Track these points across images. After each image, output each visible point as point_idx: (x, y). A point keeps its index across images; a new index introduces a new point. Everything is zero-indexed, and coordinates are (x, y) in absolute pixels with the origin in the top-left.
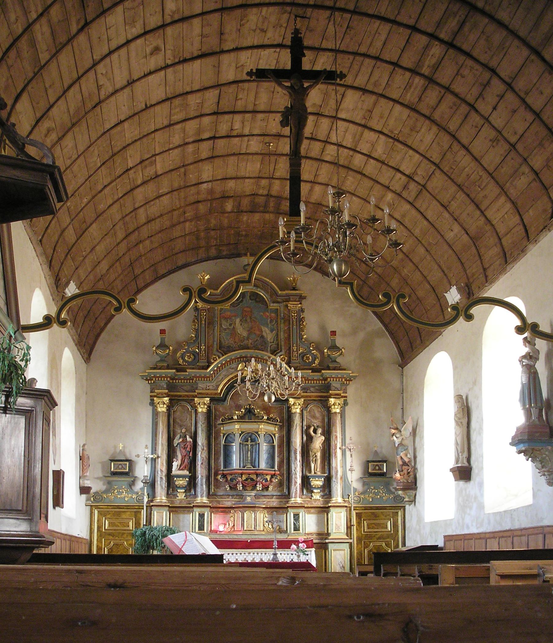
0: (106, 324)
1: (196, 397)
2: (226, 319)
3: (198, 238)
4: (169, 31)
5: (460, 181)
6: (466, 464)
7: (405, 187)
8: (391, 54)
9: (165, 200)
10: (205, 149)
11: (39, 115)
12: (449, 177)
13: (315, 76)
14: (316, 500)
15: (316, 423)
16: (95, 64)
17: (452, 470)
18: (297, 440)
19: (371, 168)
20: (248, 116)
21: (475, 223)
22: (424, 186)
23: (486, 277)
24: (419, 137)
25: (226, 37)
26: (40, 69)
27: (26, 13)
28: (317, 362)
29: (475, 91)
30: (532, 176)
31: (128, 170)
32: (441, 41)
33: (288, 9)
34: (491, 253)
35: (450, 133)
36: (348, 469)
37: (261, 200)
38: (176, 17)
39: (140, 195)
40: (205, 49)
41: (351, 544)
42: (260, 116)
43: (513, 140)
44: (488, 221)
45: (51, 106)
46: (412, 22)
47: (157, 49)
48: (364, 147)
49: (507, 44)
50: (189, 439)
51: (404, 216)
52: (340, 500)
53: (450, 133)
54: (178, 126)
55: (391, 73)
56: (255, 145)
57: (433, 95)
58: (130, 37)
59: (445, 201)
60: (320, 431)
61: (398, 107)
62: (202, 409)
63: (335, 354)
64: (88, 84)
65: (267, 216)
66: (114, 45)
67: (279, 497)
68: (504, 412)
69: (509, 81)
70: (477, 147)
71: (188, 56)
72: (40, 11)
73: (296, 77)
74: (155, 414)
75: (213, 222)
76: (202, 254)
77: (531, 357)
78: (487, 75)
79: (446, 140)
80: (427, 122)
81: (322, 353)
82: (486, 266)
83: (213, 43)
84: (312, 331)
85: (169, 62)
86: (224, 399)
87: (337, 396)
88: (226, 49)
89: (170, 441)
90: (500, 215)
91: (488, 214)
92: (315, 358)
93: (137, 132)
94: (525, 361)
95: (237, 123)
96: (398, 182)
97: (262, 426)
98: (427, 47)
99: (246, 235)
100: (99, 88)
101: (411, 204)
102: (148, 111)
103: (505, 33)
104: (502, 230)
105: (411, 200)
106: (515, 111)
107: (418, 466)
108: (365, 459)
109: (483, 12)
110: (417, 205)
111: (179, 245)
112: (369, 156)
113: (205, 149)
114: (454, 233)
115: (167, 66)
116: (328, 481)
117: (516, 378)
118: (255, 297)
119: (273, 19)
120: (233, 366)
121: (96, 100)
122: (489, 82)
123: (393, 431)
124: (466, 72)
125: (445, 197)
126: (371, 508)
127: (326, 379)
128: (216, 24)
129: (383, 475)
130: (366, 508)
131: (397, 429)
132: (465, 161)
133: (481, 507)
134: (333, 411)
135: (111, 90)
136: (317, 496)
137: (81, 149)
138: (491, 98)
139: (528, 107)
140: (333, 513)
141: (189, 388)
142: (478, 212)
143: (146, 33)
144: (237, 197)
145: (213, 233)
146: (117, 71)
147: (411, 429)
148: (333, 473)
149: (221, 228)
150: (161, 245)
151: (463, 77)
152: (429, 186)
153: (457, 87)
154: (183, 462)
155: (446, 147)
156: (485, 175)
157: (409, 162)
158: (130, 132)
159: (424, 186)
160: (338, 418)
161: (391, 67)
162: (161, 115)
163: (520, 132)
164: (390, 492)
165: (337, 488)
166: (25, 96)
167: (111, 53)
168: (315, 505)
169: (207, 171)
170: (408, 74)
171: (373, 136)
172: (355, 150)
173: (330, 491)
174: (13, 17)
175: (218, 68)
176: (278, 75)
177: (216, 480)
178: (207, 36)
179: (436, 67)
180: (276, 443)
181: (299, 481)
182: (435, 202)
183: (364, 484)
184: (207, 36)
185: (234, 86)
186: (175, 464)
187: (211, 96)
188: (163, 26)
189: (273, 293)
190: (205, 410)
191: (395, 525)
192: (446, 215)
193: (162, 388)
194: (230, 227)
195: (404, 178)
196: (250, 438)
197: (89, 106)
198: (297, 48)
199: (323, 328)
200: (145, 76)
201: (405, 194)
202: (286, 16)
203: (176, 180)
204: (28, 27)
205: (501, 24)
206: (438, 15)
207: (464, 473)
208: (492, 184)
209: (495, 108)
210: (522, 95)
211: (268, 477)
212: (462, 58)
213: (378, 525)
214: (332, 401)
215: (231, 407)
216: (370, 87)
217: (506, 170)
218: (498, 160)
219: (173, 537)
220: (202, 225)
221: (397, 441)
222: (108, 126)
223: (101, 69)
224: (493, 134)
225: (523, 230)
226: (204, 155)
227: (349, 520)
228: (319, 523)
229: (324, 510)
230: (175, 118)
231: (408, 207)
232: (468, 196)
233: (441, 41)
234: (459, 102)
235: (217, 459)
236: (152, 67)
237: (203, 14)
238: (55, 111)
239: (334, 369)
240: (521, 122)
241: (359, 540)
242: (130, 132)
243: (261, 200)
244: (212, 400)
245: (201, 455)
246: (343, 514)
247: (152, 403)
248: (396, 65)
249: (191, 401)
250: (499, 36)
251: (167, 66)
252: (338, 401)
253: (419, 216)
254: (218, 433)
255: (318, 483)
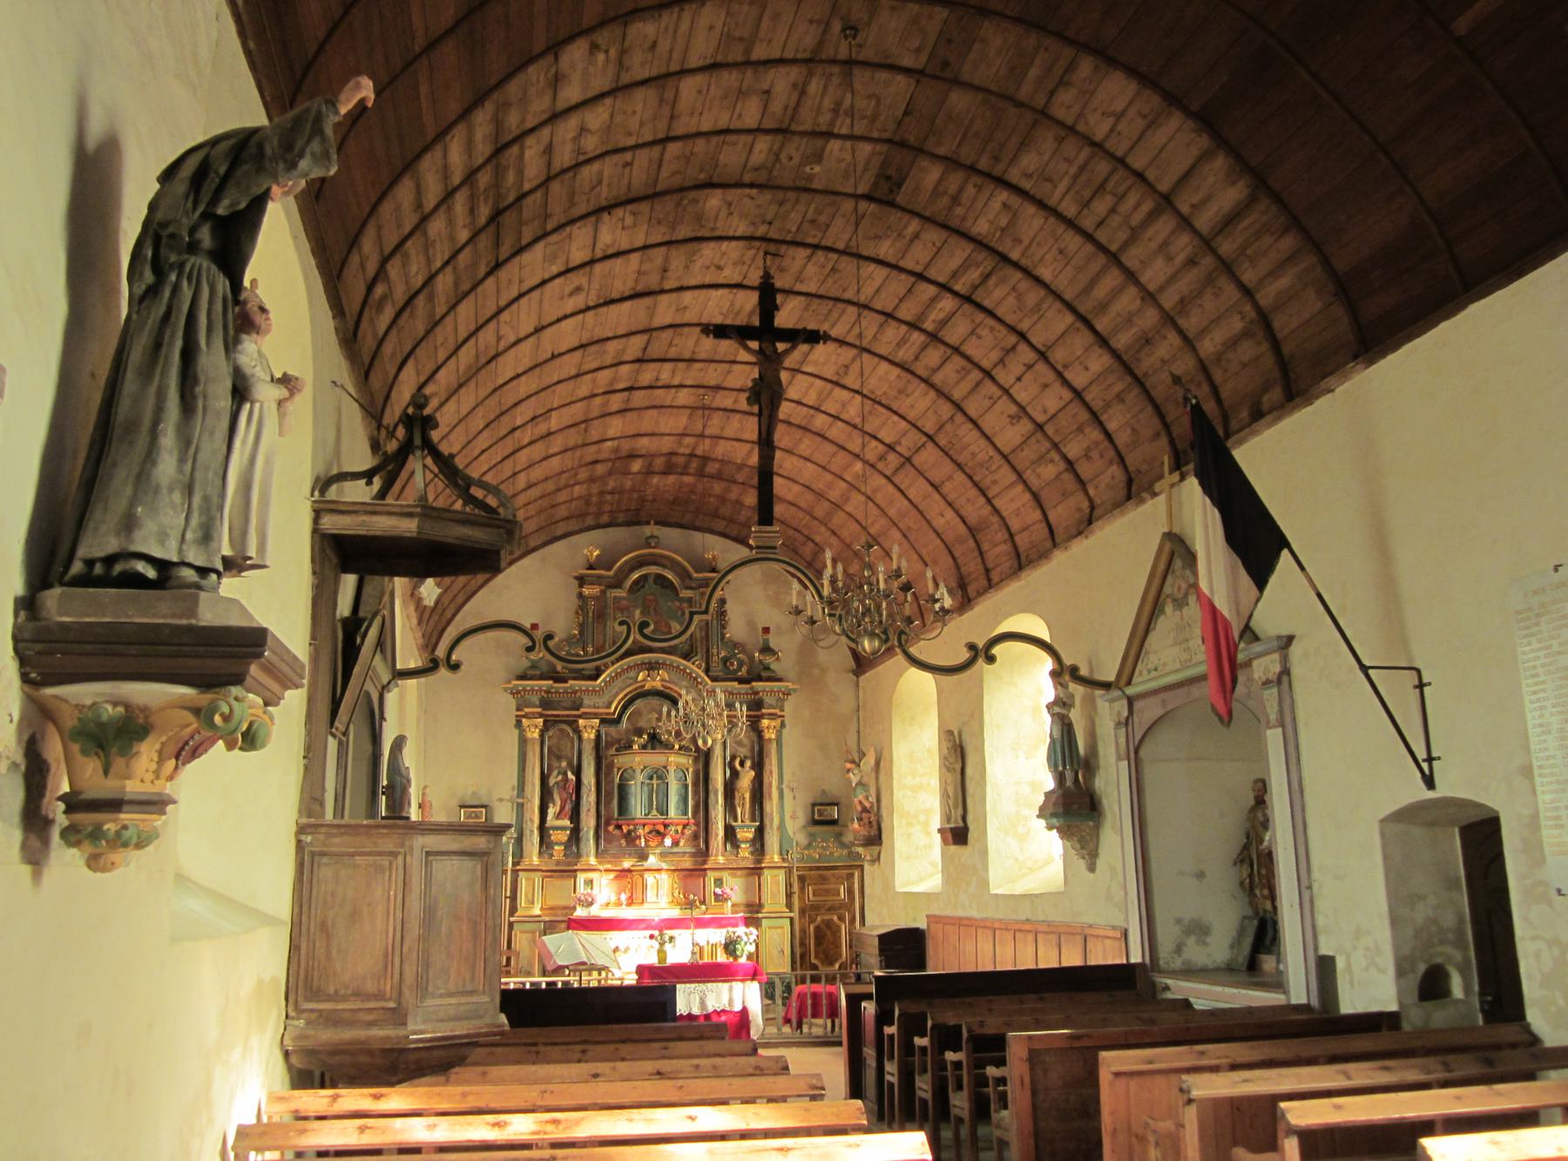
0: (454, 615)
1: (580, 716)
2: (622, 610)
3: (588, 503)
4: (598, 268)
5: (961, 459)
6: (961, 824)
7: (882, 458)
8: (885, 302)
9: (555, 461)
10: (616, 402)
11: (422, 379)
12: (946, 454)
13: (795, 336)
14: (744, 858)
15: (743, 752)
16: (500, 311)
17: (940, 831)
18: (718, 777)
19: (837, 431)
20: (680, 365)
21: (976, 509)
22: (908, 460)
23: (989, 580)
24: (908, 401)
25: (668, 274)
26: (435, 324)
27: (429, 261)
28: (744, 669)
29: (995, 356)
30: (1062, 465)
31: (514, 429)
32: (956, 294)
33: (757, 244)
34: (998, 551)
35: (953, 402)
36: (787, 814)
37: (681, 460)
38: (610, 251)
39: (523, 458)
40: (640, 288)
41: (792, 919)
42: (698, 365)
43: (1040, 418)
44: (996, 511)
45: (439, 368)
46: (919, 269)
47: (578, 289)
48: (831, 408)
49: (1045, 306)
50: (570, 775)
51: (875, 491)
52: (776, 858)
53: (953, 402)
54: (589, 376)
55: (881, 326)
56: (683, 397)
57: (934, 355)
58: (547, 276)
59: (937, 481)
60: (748, 763)
61: (885, 366)
62: (589, 736)
63: (769, 660)
64: (487, 336)
65: (686, 479)
66: (526, 286)
67: (693, 855)
68: (1019, 768)
69: (1043, 349)
70: (988, 423)
71: (615, 295)
72: (446, 257)
73: (765, 335)
74: (523, 741)
75: (611, 484)
76: (590, 521)
77: (1064, 704)
78: (1013, 339)
79: (946, 409)
80: (923, 385)
81: (752, 658)
82: (990, 565)
83: (653, 281)
84: (737, 628)
85: (591, 304)
86: (618, 721)
87: (772, 716)
88: (667, 287)
89: (544, 779)
90: (1015, 506)
91: (997, 503)
92: (741, 664)
93: (481, 340)
94: (1057, 709)
95: (665, 373)
96: (873, 450)
97: (671, 759)
98: (934, 300)
99: (654, 501)
100: (499, 339)
101: (888, 478)
102: (557, 362)
103: (1043, 292)
104: (1015, 525)
105: (888, 473)
106: (1046, 386)
107: (884, 813)
108: (810, 800)
109: (1016, 265)
110: (897, 480)
111: (562, 512)
112: (837, 418)
113: (616, 402)
114: (945, 519)
115: (588, 308)
116: (760, 831)
117: (1042, 728)
118: (661, 580)
119: (734, 255)
120: (632, 674)
121: (493, 352)
122: (1014, 348)
123: (849, 765)
124: (984, 332)
125: (936, 476)
126: (818, 868)
127: (756, 693)
128: (659, 261)
129: (833, 822)
130: (811, 869)
131: (853, 762)
132: (968, 434)
133: (985, 883)
134: (767, 736)
135: (512, 339)
136: (745, 851)
137: (464, 412)
138: (1015, 367)
139: (1066, 383)
140: (767, 875)
141: (569, 704)
142: (983, 500)
143: (568, 271)
144: (649, 457)
145: (609, 497)
146: (524, 317)
147: (872, 762)
148: (767, 821)
149: (621, 492)
150: (540, 512)
151: (979, 337)
152: (915, 460)
153: (970, 349)
154: (562, 808)
155: (945, 417)
156: (997, 457)
157: (890, 428)
158: (526, 385)
159: (908, 460)
160: (773, 747)
161: (882, 318)
162: (568, 365)
163: (1052, 411)
164: (843, 845)
165: (772, 841)
166: (411, 362)
167: (521, 296)
168: (742, 865)
169: (616, 427)
170: (904, 328)
171: (845, 394)
172: (817, 409)
173: (762, 846)
174: (414, 268)
175: (652, 311)
176: (742, 333)
177: (607, 831)
178: (644, 274)
179: (944, 323)
180: (689, 781)
181: (721, 833)
182: (921, 480)
183: (812, 836)
184: (644, 274)
185: (670, 332)
186: (551, 811)
187: (637, 343)
188: (592, 262)
189: (684, 575)
190: (592, 736)
191: (850, 892)
192: (937, 497)
193: (534, 706)
194: (633, 490)
195: (881, 447)
196: (659, 774)
197: (483, 360)
198: (768, 295)
199: (751, 624)
200: (559, 320)
201: (880, 466)
202: (753, 252)
203: (573, 437)
204: (429, 280)
205: (1038, 281)
206: (955, 263)
207: (958, 834)
208: (1006, 469)
209: (1019, 379)
210: (1060, 368)
211: (680, 828)
212: (980, 316)
213: (827, 892)
214: (765, 722)
215: (627, 731)
216: (850, 339)
217: (1029, 453)
218: (1018, 440)
219: (230, 586)
220: (595, 488)
221: (854, 780)
222: (501, 381)
223: (505, 316)
224: (1013, 409)
225: (1046, 531)
226: (614, 408)
227: (789, 885)
228: (747, 890)
229: (756, 871)
230: (586, 367)
231: (884, 481)
232: (970, 478)
233: (956, 294)
234: (969, 366)
235: (608, 802)
236: (569, 310)
237: (645, 247)
238: (442, 373)
239: (769, 679)
240: (1055, 398)
241: (802, 912)
242: (526, 385)
243: (681, 460)
244: (603, 721)
245: (589, 798)
246: (781, 876)
247: (519, 724)
248: (889, 315)
249: (573, 723)
250: (1034, 295)
251: (588, 308)
252: (773, 723)
253: (898, 494)
254: (611, 765)
255: (746, 833)
